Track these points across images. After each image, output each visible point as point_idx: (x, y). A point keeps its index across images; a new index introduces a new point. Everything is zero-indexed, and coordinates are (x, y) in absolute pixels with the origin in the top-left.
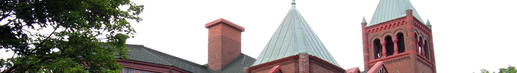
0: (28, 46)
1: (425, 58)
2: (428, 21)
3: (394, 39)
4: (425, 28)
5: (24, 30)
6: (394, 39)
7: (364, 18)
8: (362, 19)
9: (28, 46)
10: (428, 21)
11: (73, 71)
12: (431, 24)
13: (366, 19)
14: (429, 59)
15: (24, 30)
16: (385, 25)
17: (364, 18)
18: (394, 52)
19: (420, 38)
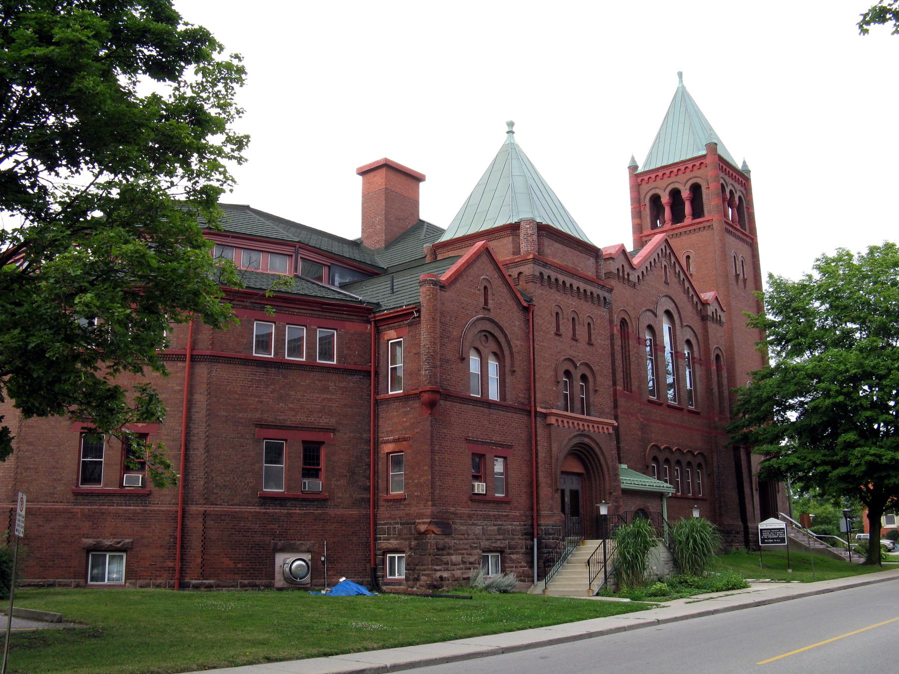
2: (744, 162)
3: (685, 194)
6: (685, 194)
7: (633, 158)
8: (629, 159)
10: (744, 162)
14: (745, 230)
17: (633, 158)
18: (684, 216)
19: (731, 192)
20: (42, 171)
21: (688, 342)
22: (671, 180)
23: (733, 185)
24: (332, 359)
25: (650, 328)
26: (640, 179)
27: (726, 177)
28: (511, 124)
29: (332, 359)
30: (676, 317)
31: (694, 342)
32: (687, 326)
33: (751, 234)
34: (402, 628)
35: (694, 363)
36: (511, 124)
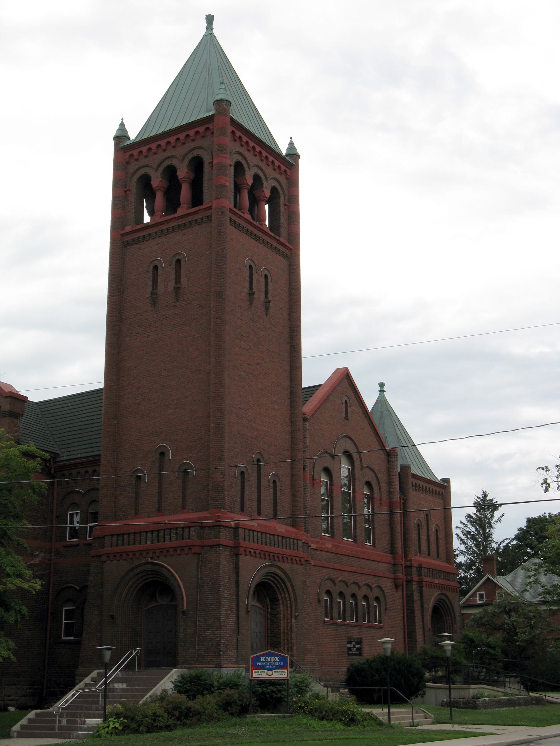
0: (548, 517)
1: (248, 216)
2: (291, 144)
3: (183, 172)
4: (261, 147)
5: (336, 569)
6: (183, 172)
7: (122, 125)
8: (117, 127)
9: (548, 517)
10: (291, 144)
11: (89, 593)
12: (299, 152)
13: (127, 127)
14: (279, 235)
15: (336, 569)
16: (167, 140)
17: (122, 125)
18: (179, 205)
19: (256, 178)
20: (132, 533)
21: (368, 484)
22: (168, 154)
23: (258, 166)
24: (70, 539)
25: (327, 471)
26: (129, 154)
27: (263, 165)
28: (382, 385)
29: (70, 539)
30: (355, 457)
31: (374, 483)
32: (368, 467)
33: (290, 242)
34: (137, 744)
35: (373, 502)
36: (382, 385)
